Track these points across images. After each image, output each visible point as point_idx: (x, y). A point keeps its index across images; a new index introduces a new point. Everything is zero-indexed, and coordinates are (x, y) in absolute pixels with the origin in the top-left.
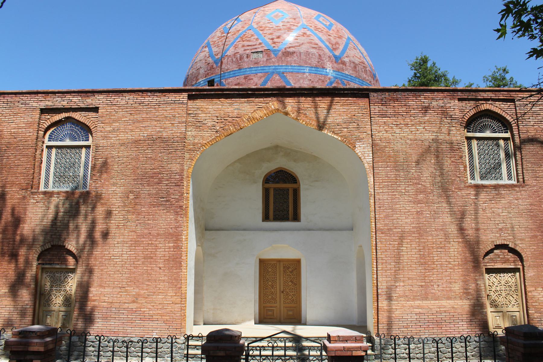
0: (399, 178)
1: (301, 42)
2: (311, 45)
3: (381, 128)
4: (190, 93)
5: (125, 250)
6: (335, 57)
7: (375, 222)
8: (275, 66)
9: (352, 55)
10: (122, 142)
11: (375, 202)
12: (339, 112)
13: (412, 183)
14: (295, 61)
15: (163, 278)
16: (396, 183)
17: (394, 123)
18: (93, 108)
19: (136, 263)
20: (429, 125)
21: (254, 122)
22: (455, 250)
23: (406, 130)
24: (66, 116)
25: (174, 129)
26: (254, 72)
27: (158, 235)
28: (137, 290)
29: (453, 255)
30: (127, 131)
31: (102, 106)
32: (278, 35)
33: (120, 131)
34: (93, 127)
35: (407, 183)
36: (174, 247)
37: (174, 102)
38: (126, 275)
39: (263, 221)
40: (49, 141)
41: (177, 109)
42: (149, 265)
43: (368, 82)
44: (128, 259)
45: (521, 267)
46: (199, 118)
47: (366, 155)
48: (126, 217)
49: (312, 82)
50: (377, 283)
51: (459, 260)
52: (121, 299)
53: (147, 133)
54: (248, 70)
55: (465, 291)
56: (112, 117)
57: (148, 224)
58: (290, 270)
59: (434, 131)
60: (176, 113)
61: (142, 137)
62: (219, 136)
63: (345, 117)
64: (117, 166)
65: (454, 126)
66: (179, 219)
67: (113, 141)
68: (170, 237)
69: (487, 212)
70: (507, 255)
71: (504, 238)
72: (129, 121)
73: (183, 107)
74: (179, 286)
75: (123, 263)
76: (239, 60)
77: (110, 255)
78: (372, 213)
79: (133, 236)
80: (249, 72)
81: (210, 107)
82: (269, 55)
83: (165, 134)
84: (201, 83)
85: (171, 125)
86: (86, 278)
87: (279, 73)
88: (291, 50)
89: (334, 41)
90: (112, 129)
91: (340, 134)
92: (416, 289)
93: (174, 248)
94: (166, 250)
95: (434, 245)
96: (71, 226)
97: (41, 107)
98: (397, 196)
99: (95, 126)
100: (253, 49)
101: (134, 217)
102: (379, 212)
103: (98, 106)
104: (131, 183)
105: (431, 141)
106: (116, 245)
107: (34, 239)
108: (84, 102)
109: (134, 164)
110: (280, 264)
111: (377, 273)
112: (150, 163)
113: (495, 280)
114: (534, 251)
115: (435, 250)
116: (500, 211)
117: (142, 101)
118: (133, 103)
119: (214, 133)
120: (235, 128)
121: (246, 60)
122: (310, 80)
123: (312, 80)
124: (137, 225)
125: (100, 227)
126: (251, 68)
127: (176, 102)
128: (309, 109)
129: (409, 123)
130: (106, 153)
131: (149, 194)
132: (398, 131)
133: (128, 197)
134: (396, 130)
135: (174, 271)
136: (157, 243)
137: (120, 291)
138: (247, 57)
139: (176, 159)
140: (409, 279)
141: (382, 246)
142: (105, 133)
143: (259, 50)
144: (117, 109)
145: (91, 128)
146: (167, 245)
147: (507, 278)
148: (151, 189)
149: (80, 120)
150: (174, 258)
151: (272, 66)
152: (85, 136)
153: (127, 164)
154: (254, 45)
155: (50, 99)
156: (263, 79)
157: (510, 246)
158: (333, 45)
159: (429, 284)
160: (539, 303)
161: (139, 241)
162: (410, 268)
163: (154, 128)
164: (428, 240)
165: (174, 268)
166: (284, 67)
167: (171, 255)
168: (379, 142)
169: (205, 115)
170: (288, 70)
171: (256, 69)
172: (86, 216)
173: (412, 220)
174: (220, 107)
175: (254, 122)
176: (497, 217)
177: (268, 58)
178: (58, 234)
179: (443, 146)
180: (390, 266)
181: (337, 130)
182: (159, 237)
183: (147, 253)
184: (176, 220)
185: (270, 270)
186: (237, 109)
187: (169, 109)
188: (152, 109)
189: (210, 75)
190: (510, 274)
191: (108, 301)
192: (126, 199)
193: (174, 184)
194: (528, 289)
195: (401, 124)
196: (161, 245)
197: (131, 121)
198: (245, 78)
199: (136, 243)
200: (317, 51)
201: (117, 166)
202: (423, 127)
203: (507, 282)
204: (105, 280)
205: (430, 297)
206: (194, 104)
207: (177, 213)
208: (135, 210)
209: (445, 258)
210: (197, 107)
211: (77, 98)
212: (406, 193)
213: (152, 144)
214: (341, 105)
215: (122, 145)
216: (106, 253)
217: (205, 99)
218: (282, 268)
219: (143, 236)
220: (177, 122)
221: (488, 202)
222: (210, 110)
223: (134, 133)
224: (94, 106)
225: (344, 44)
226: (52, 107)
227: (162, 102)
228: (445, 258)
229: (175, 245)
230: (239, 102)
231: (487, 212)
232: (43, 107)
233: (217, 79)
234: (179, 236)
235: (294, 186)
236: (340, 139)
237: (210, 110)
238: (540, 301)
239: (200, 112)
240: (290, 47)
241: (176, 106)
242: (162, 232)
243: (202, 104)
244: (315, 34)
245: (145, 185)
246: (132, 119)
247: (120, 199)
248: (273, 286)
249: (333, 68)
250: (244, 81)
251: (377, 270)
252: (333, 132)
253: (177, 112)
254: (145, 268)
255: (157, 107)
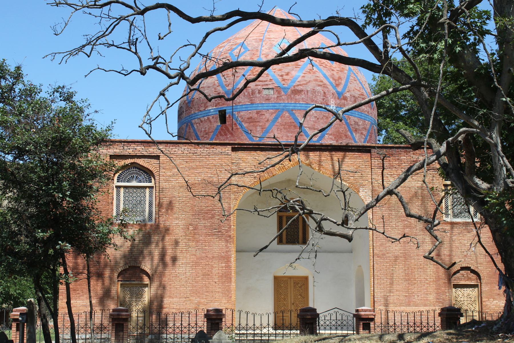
0: (391, 216)
1: (308, 80)
2: (317, 83)
4: (233, 146)
5: (188, 269)
6: (337, 94)
7: (373, 249)
8: (285, 103)
9: (353, 89)
10: (181, 185)
11: (373, 234)
12: (348, 164)
13: (400, 220)
14: (303, 99)
15: (218, 290)
16: (389, 219)
17: (389, 174)
19: (197, 279)
21: (283, 170)
22: (431, 270)
24: (132, 162)
26: (266, 108)
27: (213, 257)
28: (198, 299)
29: (429, 274)
32: (286, 72)
34: (156, 171)
36: (226, 267)
38: (190, 288)
39: (278, 244)
40: (117, 182)
41: (223, 159)
42: (207, 281)
43: (366, 113)
44: (190, 276)
45: (479, 284)
46: (240, 166)
47: (367, 198)
48: (188, 244)
49: (318, 118)
50: (374, 293)
51: (434, 278)
52: (186, 306)
54: (260, 105)
55: (437, 300)
57: (205, 249)
58: (299, 285)
59: (419, 180)
60: (223, 162)
62: (257, 181)
63: (352, 168)
64: (178, 204)
66: (229, 245)
68: (222, 259)
69: (456, 242)
70: (470, 275)
71: (467, 262)
73: (228, 158)
74: (230, 295)
75: (186, 279)
76: (251, 94)
77: (176, 273)
78: (371, 242)
79: (194, 258)
80: (261, 108)
81: (249, 158)
82: (279, 93)
84: (212, 111)
86: (159, 292)
87: (288, 111)
88: (300, 88)
89: (336, 76)
92: (402, 298)
93: (226, 268)
94: (220, 269)
95: (416, 267)
96: (146, 252)
97: (110, 154)
98: (390, 230)
99: (157, 170)
100: (264, 85)
101: (194, 244)
102: (376, 241)
104: (190, 217)
105: (417, 188)
106: (181, 266)
107: (116, 262)
109: (192, 202)
110: (290, 280)
111: (374, 286)
112: (204, 202)
113: (460, 293)
114: (489, 272)
115: (416, 270)
116: (466, 242)
117: (195, 151)
119: (253, 178)
120: (269, 175)
121: (258, 95)
122: (316, 117)
123: (318, 117)
124: (196, 250)
125: (170, 252)
126: (262, 104)
128: (325, 161)
130: (169, 193)
131: (205, 227)
133: (188, 229)
135: (226, 284)
136: (212, 263)
137: (185, 300)
138: (259, 93)
139: (225, 199)
140: (397, 291)
141: (378, 266)
142: (167, 177)
143: (270, 87)
145: (154, 172)
146: (220, 265)
147: (469, 291)
148: (206, 223)
149: (144, 165)
150: (226, 275)
151: (282, 103)
152: (148, 178)
153: (186, 202)
154: (265, 81)
155: (117, 147)
156: (274, 115)
157: (472, 268)
158: (335, 80)
159: (411, 295)
160: (490, 310)
161: (198, 262)
162: (398, 283)
164: (411, 262)
165: (226, 282)
166: (293, 105)
167: (223, 273)
168: (378, 188)
169: (245, 164)
170: (296, 108)
171: (267, 105)
172: (157, 244)
173: (400, 248)
175: (283, 170)
176: (463, 246)
177: (279, 95)
178: (134, 257)
179: (425, 192)
180: (383, 281)
181: (346, 178)
182: (214, 259)
183: (205, 271)
184: (227, 246)
185: (282, 285)
188: (203, 159)
189: (222, 105)
190: (471, 289)
191: (176, 308)
192: (187, 230)
194: (483, 300)
195: (394, 174)
196: (215, 265)
198: (258, 113)
199: (196, 264)
200: (322, 88)
201: (178, 204)
203: (469, 295)
204: (173, 292)
205: (411, 304)
206: (236, 155)
207: (227, 241)
208: (194, 238)
209: (424, 276)
210: (239, 157)
212: (396, 228)
214: (349, 159)
216: (173, 271)
217: (245, 151)
218: (292, 284)
219: (201, 258)
221: (457, 235)
222: (249, 160)
223: (190, 178)
224: (156, 155)
225: (345, 78)
226: (120, 154)
227: (212, 153)
228: (424, 276)
229: (227, 265)
230: (271, 154)
231: (456, 242)
232: (112, 154)
233: (229, 111)
234: (229, 258)
237: (249, 160)
238: (491, 309)
239: (241, 162)
240: (298, 85)
242: (216, 255)
243: (242, 155)
244: (320, 70)
245: (201, 219)
246: (187, 166)
247: (182, 230)
248: (285, 299)
249: (335, 104)
250: (256, 116)
251: (374, 284)
253: (224, 162)
254: (204, 283)
255: (208, 157)
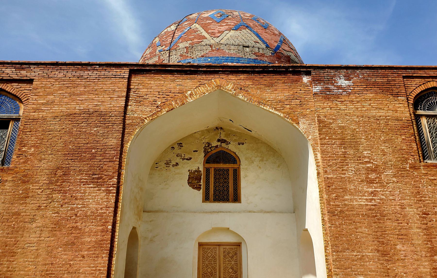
3: (325, 104)
4: (132, 68)
18: (27, 80)
20: (375, 102)
23: (351, 107)
25: (113, 103)
30: (62, 103)
31: (37, 78)
33: (55, 103)
35: (357, 161)
37: (114, 76)
39: (203, 202)
46: (140, 93)
48: (51, 196)
53: (83, 106)
56: (48, 90)
58: (231, 255)
61: (78, 111)
63: (288, 94)
64: (46, 141)
65: (402, 103)
67: (45, 113)
72: (65, 94)
81: (152, 82)
83: (103, 108)
85: (109, 99)
90: (45, 101)
91: (282, 111)
99: (27, 98)
103: (32, 78)
108: (18, 74)
112: (84, 137)
118: (71, 76)
127: (116, 76)
129: (354, 100)
132: (343, 107)
134: (341, 107)
144: (54, 82)
163: (91, 101)
169: (146, 90)
174: (163, 82)
186: (180, 85)
187: (109, 83)
188: (90, 83)
193: (108, 160)
197: (67, 94)
202: (369, 104)
206: (136, 79)
211: (10, 70)
213: (88, 118)
215: (55, 118)
220: (117, 96)
223: (70, 106)
224: (28, 78)
227: (102, 76)
235: (235, 166)
236: (282, 115)
239: (141, 87)
241: (117, 81)
252: (275, 109)
255: (97, 81)
